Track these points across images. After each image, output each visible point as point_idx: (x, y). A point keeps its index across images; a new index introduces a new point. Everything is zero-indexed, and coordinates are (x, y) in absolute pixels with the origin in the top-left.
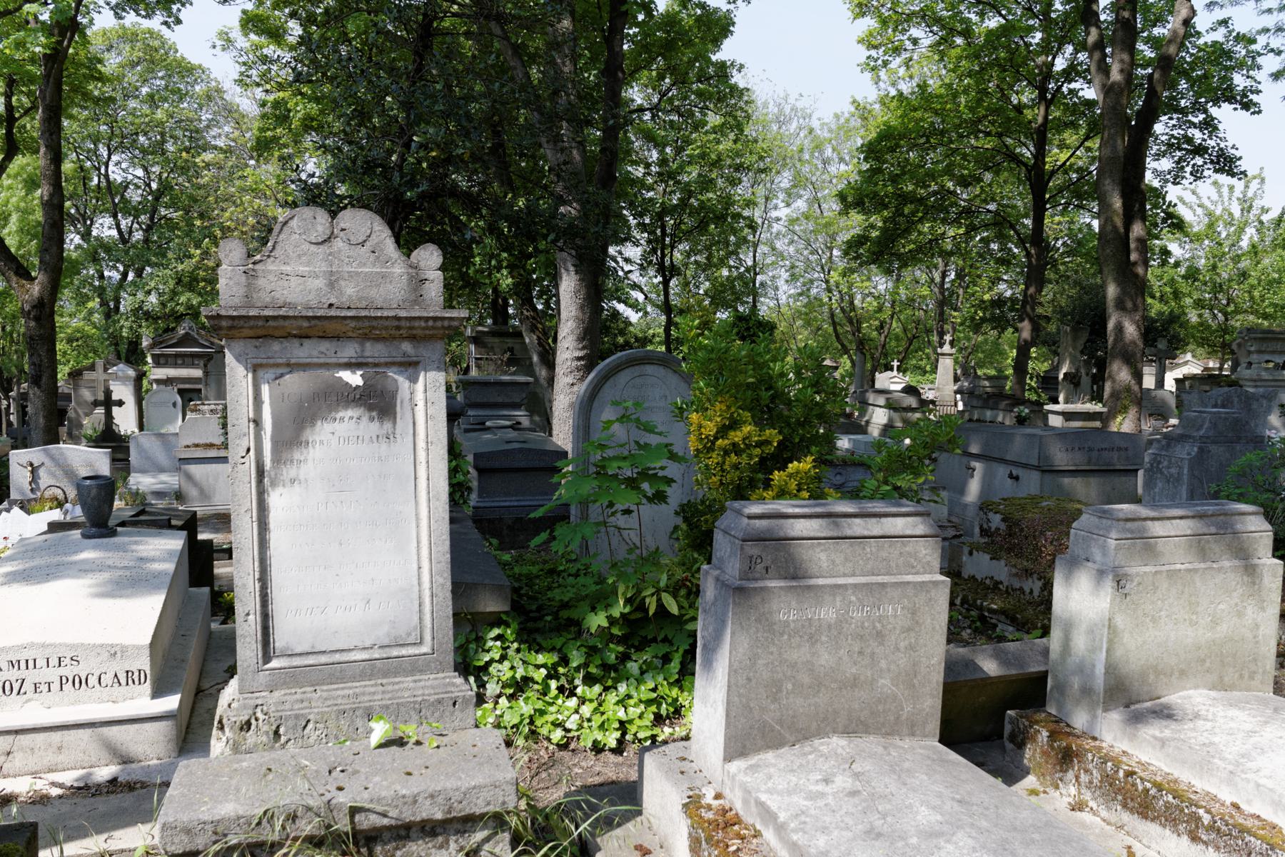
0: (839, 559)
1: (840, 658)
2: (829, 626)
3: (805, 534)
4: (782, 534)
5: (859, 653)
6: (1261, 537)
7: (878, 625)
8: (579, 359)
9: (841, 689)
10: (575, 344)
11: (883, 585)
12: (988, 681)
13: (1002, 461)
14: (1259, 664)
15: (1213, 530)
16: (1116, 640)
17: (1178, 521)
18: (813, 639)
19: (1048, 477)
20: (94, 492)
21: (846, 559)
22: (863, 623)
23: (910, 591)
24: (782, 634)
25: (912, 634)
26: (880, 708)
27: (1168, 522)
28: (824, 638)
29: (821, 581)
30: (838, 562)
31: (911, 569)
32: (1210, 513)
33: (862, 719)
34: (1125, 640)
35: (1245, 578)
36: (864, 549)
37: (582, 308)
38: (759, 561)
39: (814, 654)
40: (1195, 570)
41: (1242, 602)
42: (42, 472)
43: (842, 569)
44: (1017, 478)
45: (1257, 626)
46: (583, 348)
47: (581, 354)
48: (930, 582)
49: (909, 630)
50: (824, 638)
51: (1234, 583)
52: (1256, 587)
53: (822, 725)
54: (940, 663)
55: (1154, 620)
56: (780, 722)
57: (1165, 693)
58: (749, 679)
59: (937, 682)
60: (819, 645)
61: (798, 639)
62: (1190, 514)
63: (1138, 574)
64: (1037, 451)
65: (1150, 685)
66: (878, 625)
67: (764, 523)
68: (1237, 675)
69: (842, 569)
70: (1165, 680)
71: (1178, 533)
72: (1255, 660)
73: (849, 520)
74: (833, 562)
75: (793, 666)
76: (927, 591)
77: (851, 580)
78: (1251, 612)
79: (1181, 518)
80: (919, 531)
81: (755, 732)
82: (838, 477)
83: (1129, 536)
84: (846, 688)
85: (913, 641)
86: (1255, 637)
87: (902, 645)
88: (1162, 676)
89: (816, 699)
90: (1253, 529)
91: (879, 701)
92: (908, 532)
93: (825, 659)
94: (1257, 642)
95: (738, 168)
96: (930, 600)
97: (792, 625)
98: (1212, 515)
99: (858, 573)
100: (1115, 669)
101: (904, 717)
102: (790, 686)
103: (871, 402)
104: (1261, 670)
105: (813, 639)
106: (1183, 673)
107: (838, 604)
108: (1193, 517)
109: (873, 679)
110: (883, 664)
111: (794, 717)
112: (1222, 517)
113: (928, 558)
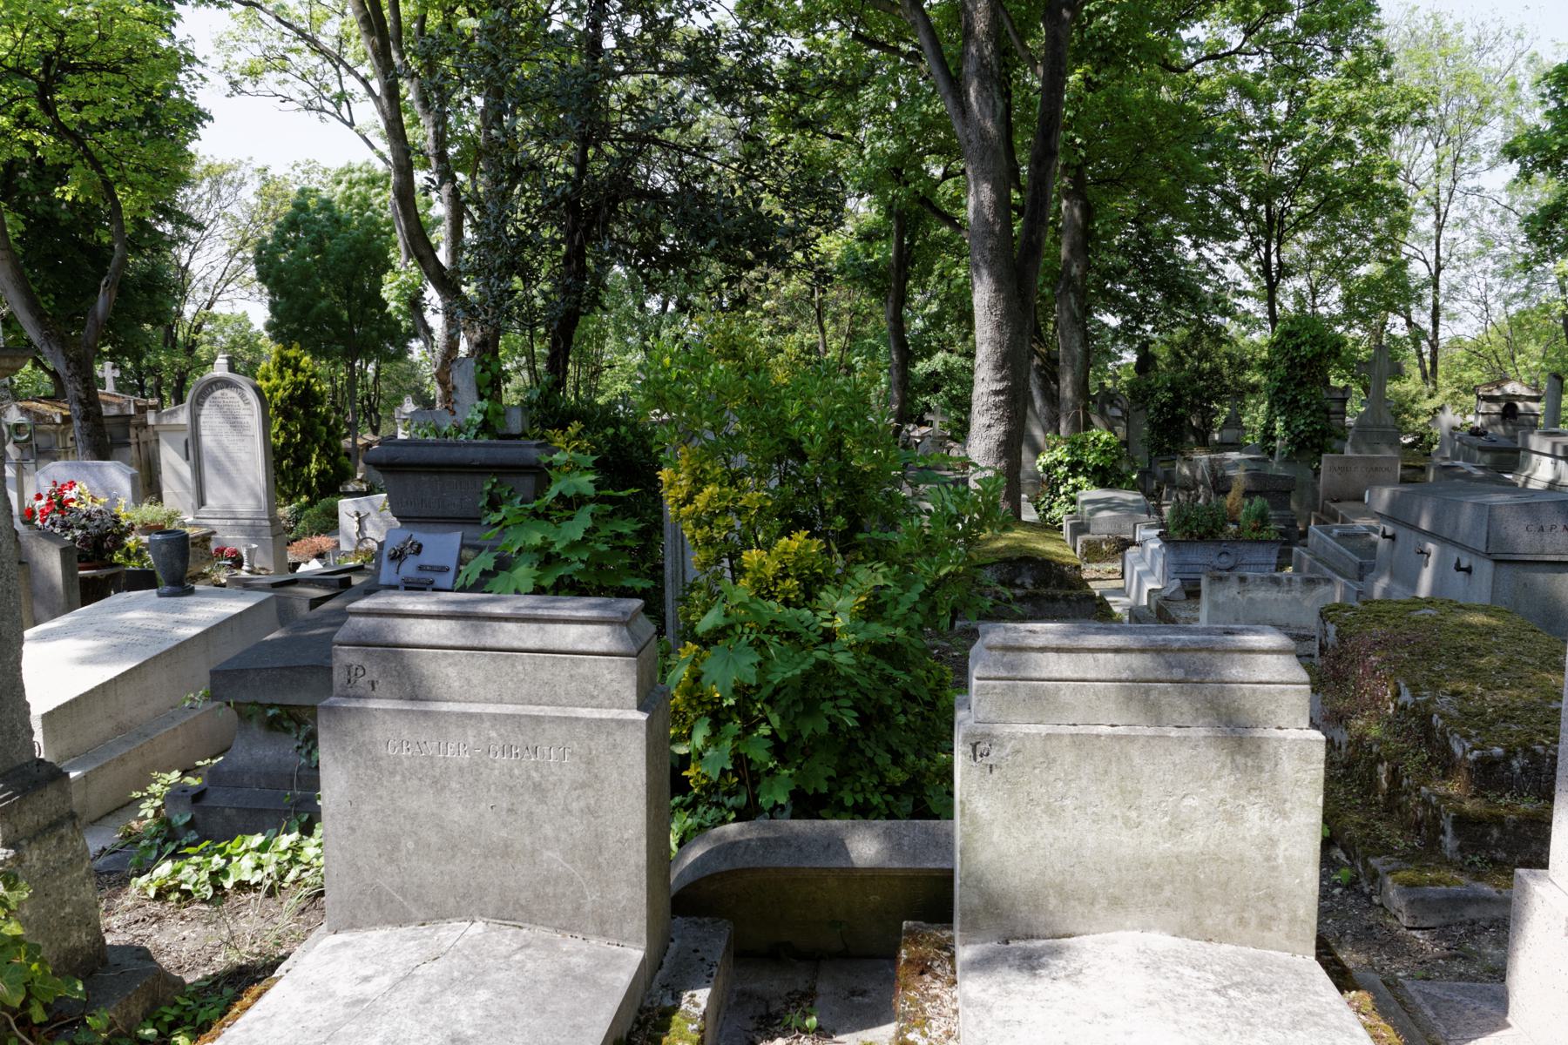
0: (477, 677)
1: (482, 815)
2: (461, 769)
3: (425, 640)
4: (391, 638)
5: (509, 810)
6: (1283, 692)
7: (534, 774)
8: (996, 393)
9: (486, 857)
10: (991, 373)
11: (538, 720)
12: (872, 876)
13: (1455, 544)
14: (1281, 905)
15: (1178, 674)
16: (976, 836)
17: (1110, 655)
18: (439, 785)
19: (1506, 571)
20: (164, 548)
21: (488, 679)
22: (511, 770)
23: (581, 732)
24: (393, 774)
25: (590, 793)
26: (549, 890)
27: (1089, 656)
28: (454, 785)
29: (444, 707)
30: (475, 681)
31: (589, 700)
32: (1177, 645)
33: (523, 902)
34: (995, 838)
35: (1240, 759)
36: (513, 666)
37: (999, 326)
38: (360, 672)
39: (441, 805)
40: (1131, 739)
41: (1235, 798)
42: (367, 524)
43: (482, 692)
44: (1468, 570)
45: (1273, 842)
46: (1002, 379)
47: (999, 386)
48: (612, 720)
49: (583, 786)
50: (454, 785)
51: (1215, 766)
52: (1266, 776)
53: (463, 903)
54: (638, 839)
55: (1049, 810)
56: (402, 890)
57: (1081, 929)
58: (352, 829)
59: (637, 866)
60: (448, 793)
61: (416, 782)
62: (1136, 645)
63: (1012, 737)
64: (1485, 528)
65: (1052, 913)
66: (534, 774)
67: (372, 621)
68: (1231, 918)
69: (482, 692)
70: (1080, 909)
71: (1103, 676)
72: (1271, 897)
73: (496, 625)
74: (468, 681)
75: (413, 817)
76: (609, 734)
77: (492, 709)
78: (1255, 818)
79: (1117, 651)
80: (598, 646)
81: (368, 899)
82: (1224, 558)
83: (1005, 674)
84: (494, 857)
85: (592, 802)
86: (1268, 859)
87: (575, 806)
88: (1073, 903)
89: (450, 867)
90: (1265, 677)
91: (547, 881)
92: (582, 647)
93: (458, 814)
94: (1274, 868)
95: (1383, 123)
96: (614, 746)
97: (406, 763)
98: (1181, 650)
99: (506, 698)
100: (980, 881)
101: (588, 908)
102: (411, 845)
103: (1534, 448)
104: (1285, 916)
105: (439, 785)
106: (1115, 902)
107: (471, 740)
108: (1142, 651)
109: (534, 851)
110: (548, 830)
111: (419, 886)
112: (1204, 655)
113: (616, 686)
